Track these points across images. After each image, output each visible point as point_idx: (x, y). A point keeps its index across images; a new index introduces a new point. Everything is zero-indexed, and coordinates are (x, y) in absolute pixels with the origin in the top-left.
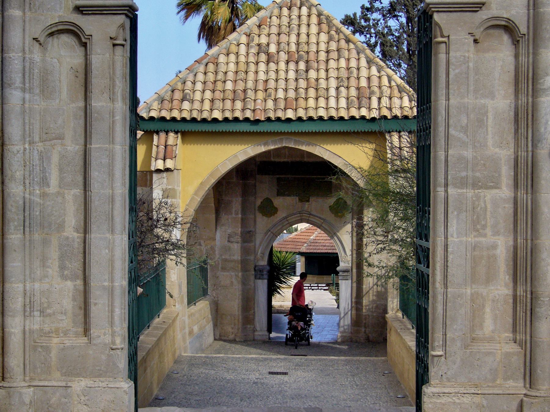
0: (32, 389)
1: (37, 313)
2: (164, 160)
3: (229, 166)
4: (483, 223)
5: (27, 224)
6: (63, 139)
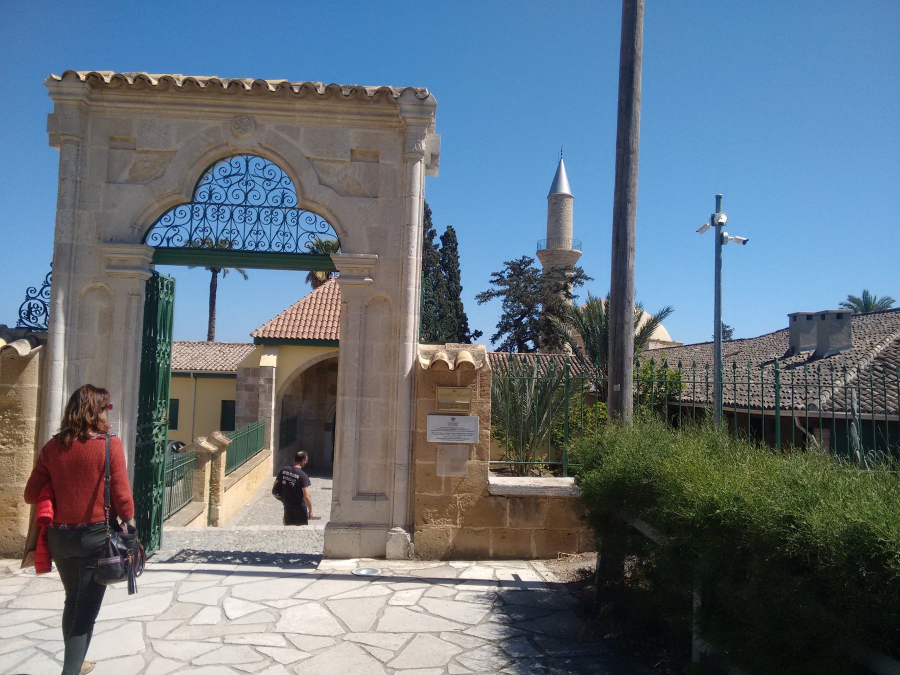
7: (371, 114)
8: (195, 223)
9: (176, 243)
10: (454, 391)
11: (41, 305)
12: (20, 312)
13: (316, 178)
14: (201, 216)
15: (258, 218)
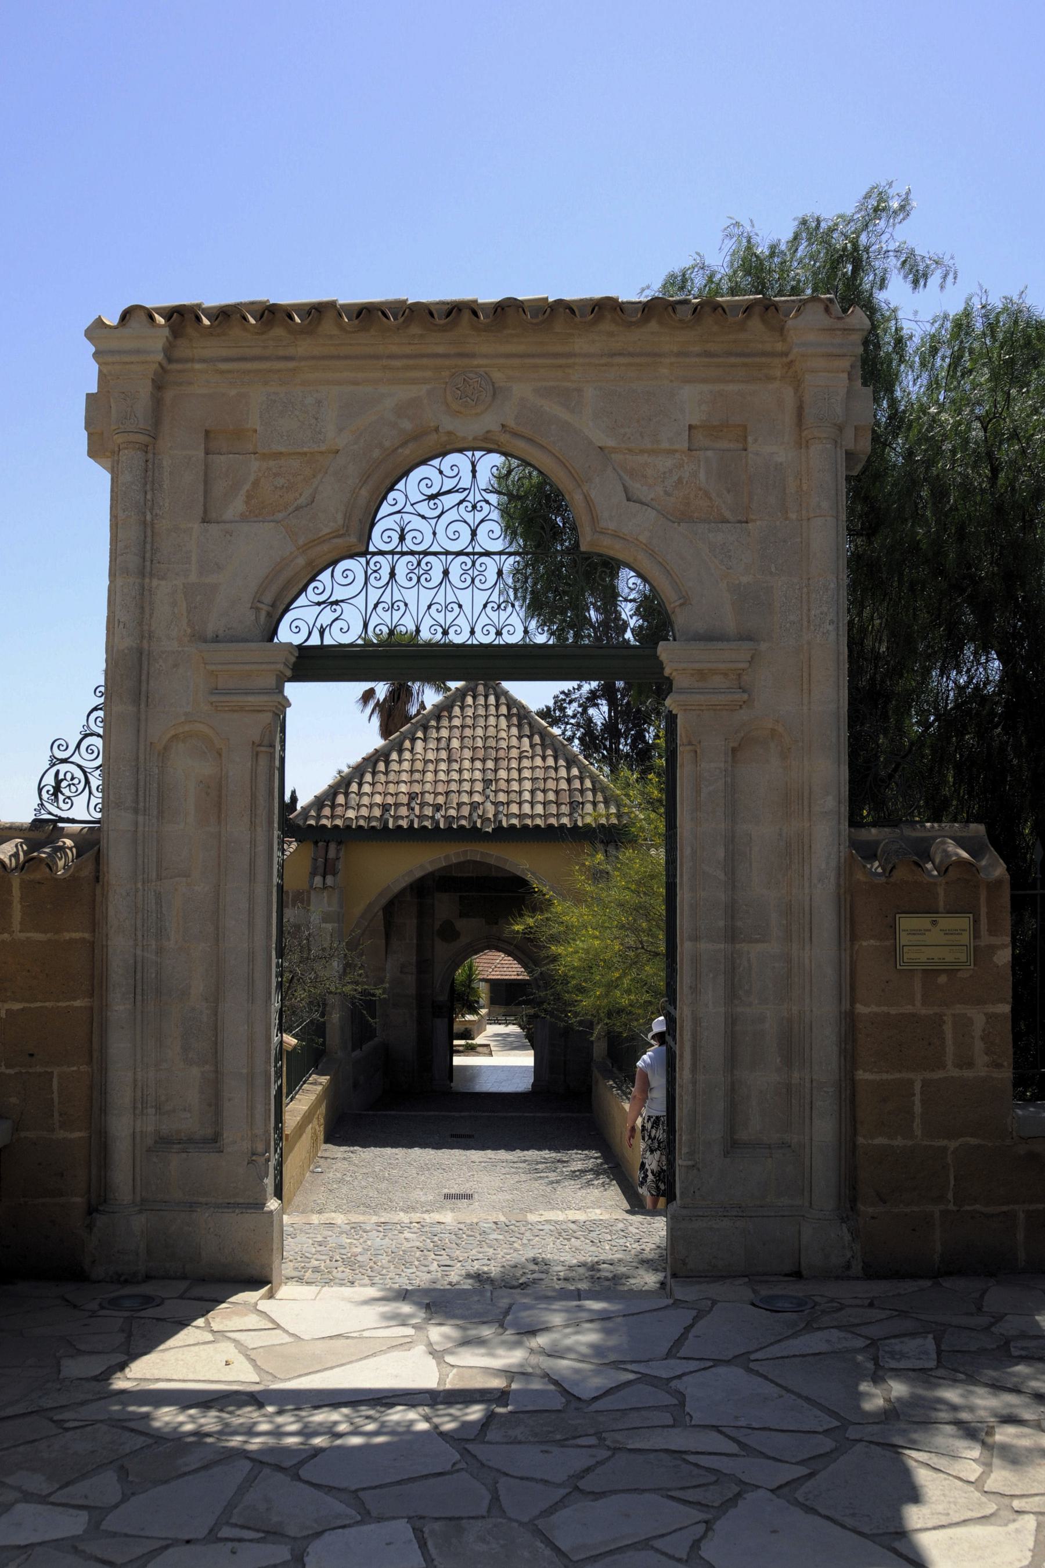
1: (151, 1111)
4: (747, 987)
5: (139, 990)
6: (189, 876)
7: (729, 354)
8: (374, 595)
9: (335, 637)
10: (934, 923)
11: (79, 774)
12: (40, 790)
13: (620, 488)
14: (386, 577)
15: (392, 574)
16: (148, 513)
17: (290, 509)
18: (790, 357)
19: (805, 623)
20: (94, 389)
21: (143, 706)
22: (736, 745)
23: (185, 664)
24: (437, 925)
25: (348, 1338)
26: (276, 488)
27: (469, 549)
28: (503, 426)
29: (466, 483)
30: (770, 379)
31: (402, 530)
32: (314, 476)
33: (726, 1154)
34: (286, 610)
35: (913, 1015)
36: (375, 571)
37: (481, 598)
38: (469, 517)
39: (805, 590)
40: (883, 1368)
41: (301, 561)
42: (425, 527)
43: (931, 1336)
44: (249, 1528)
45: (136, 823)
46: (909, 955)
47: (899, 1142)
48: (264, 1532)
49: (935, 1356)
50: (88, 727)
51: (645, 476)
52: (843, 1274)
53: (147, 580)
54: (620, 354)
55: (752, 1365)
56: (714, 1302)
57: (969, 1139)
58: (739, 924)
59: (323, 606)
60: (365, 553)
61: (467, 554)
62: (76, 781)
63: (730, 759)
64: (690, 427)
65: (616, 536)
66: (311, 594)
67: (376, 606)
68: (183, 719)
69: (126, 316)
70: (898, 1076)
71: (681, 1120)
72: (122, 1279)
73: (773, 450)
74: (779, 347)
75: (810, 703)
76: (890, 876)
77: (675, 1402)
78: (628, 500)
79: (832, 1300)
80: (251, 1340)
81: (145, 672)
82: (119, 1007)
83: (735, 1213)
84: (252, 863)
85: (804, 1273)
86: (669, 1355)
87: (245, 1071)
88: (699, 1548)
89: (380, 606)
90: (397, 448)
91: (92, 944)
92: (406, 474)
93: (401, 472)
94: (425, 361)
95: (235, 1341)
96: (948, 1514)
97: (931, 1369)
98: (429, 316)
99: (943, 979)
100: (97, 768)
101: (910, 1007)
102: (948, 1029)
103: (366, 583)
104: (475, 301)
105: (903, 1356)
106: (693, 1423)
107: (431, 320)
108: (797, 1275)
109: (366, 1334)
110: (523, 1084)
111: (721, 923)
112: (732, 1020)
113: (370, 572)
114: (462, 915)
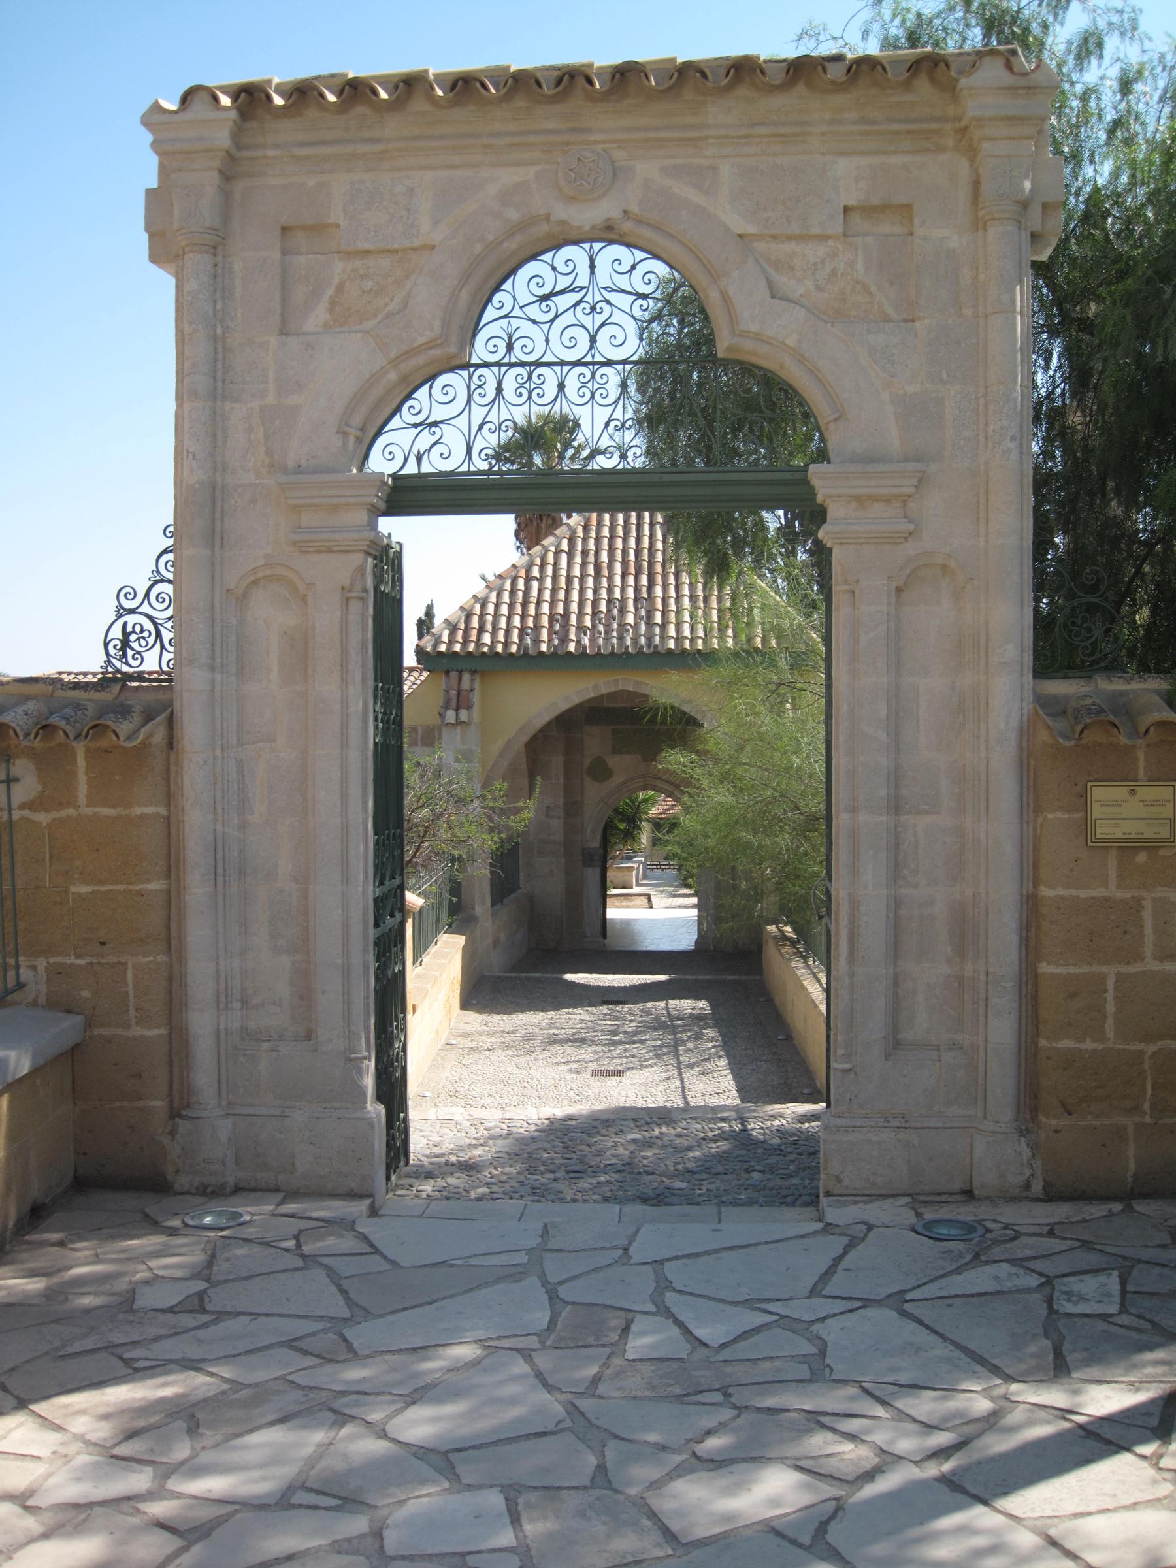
0: (231, 1120)
1: (238, 1005)
2: (457, 710)
3: (547, 718)
4: (912, 866)
5: (220, 871)
6: (273, 741)
8: (478, 414)
10: (1133, 792)
11: (148, 625)
12: (106, 645)
14: (491, 393)
15: (499, 390)
16: (219, 326)
17: (380, 317)
18: (963, 124)
19: (982, 439)
20: (154, 184)
21: (217, 548)
22: (900, 583)
23: (265, 498)
24: (587, 762)
25: (452, 1266)
26: (364, 292)
27: (589, 359)
28: (625, 212)
29: (583, 280)
30: (940, 149)
31: (510, 337)
32: (407, 277)
33: (887, 1057)
34: (379, 433)
35: (1107, 899)
36: (479, 386)
37: (602, 415)
38: (587, 321)
39: (982, 401)
40: (1057, 1312)
41: (393, 376)
42: (537, 334)
43: (1115, 1273)
44: (324, 1494)
45: (213, 682)
46: (1103, 830)
47: (1089, 1045)
48: (340, 1498)
49: (1117, 1299)
50: (158, 572)
51: (792, 269)
52: (1022, 1195)
53: (219, 403)
54: (763, 124)
55: (907, 1307)
56: (870, 1227)
57: (1169, 1042)
58: (904, 792)
59: (420, 428)
60: (466, 366)
61: (586, 364)
62: (146, 634)
63: (893, 600)
64: (846, 209)
65: (758, 338)
66: (407, 414)
67: (481, 427)
68: (262, 563)
69: (186, 98)
70: (1085, 969)
71: (836, 1017)
72: (209, 1190)
73: (942, 234)
74: (951, 110)
75: (987, 534)
76: (1080, 738)
77: (814, 1350)
78: (773, 297)
79: (1006, 1227)
80: (345, 1267)
81: (218, 509)
82: (197, 890)
83: (897, 1124)
84: (344, 726)
85: (976, 1192)
86: (814, 1292)
87: (340, 961)
88: (826, 1532)
89: (486, 427)
90: (502, 242)
91: (168, 819)
92: (513, 272)
93: (528, 254)
94: (532, 138)
95: (327, 1268)
96: (1115, 1495)
97: (1112, 1315)
98: (535, 87)
99: (1141, 857)
100: (169, 619)
101: (1103, 890)
102: (1147, 915)
103: (469, 401)
104: (591, 65)
105: (1082, 1298)
106: (833, 1377)
107: (540, 90)
108: (969, 1194)
109: (473, 1261)
110: (686, 940)
111: (883, 793)
112: (897, 904)
113: (473, 387)
114: (615, 751)
